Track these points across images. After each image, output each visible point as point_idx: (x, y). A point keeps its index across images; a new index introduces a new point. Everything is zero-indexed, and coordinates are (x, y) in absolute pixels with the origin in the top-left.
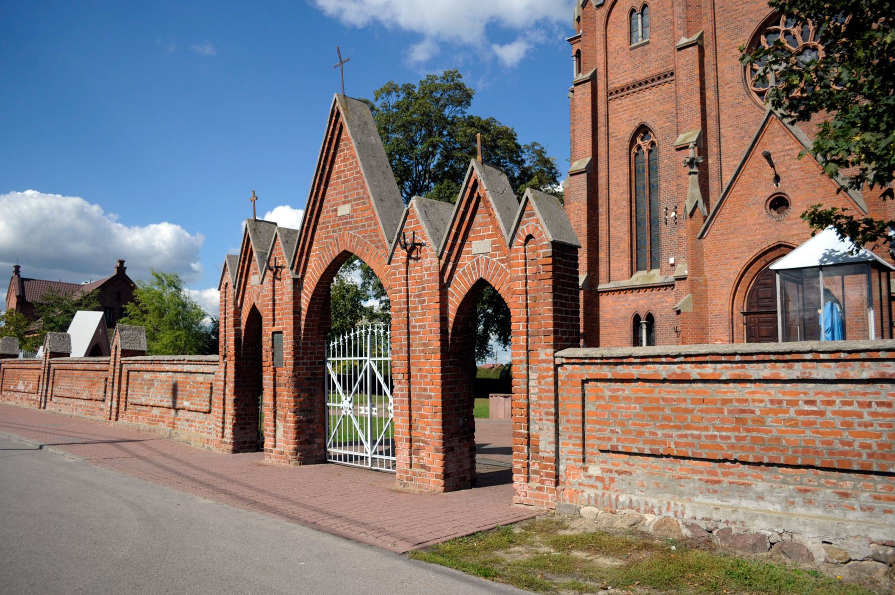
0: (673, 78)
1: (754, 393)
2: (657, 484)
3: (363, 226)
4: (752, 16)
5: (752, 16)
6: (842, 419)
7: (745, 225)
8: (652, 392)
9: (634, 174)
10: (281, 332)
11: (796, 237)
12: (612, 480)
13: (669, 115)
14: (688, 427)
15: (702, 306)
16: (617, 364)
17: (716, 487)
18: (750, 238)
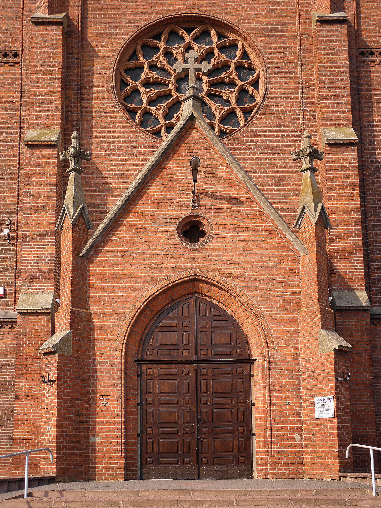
0: (18, 60)
4: (130, 18)
5: (130, 18)
7: (148, 249)
9: (188, 21)
11: (217, 272)
13: (6, 106)
15: (84, 348)
18: (154, 266)
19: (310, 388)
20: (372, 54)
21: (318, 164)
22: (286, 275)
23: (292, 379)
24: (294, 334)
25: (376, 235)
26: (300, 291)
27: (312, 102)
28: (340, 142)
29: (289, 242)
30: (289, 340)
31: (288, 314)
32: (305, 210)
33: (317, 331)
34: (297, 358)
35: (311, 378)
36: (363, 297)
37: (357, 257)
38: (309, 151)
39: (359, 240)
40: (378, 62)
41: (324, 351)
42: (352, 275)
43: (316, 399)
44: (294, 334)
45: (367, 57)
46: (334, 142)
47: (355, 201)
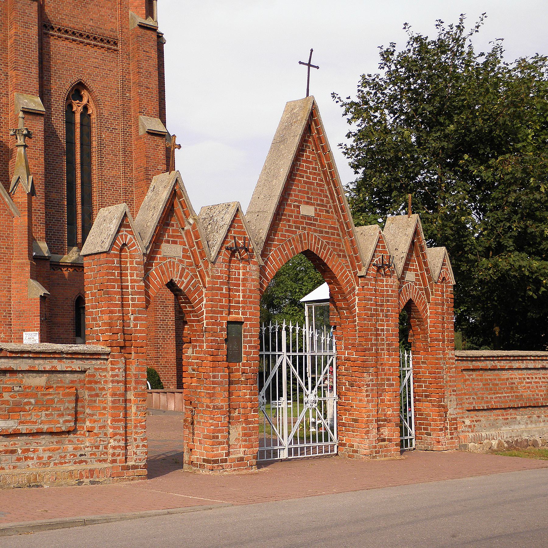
1: (512, 374)
2: (490, 424)
3: (327, 233)
6: (95, 379)
8: (481, 375)
10: (242, 323)
12: (474, 426)
14: (497, 393)
16: (473, 360)
17: (507, 421)
19: (20, 325)
20: (52, 28)
21: (29, 142)
22: (3, 231)
23: (6, 316)
24: (8, 280)
25: (50, 192)
26: (13, 246)
27: (6, 63)
28: (32, 111)
29: (7, 205)
30: (4, 285)
31: (4, 264)
32: (20, 180)
33: (27, 280)
34: (10, 300)
35: (20, 316)
36: (45, 248)
37: (41, 213)
38: (25, 132)
39: (43, 199)
40: (57, 38)
41: (32, 296)
42: (37, 228)
43: (24, 333)
44: (8, 280)
45: (48, 30)
46: (28, 110)
47: (40, 164)
